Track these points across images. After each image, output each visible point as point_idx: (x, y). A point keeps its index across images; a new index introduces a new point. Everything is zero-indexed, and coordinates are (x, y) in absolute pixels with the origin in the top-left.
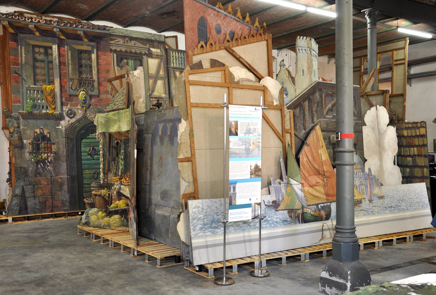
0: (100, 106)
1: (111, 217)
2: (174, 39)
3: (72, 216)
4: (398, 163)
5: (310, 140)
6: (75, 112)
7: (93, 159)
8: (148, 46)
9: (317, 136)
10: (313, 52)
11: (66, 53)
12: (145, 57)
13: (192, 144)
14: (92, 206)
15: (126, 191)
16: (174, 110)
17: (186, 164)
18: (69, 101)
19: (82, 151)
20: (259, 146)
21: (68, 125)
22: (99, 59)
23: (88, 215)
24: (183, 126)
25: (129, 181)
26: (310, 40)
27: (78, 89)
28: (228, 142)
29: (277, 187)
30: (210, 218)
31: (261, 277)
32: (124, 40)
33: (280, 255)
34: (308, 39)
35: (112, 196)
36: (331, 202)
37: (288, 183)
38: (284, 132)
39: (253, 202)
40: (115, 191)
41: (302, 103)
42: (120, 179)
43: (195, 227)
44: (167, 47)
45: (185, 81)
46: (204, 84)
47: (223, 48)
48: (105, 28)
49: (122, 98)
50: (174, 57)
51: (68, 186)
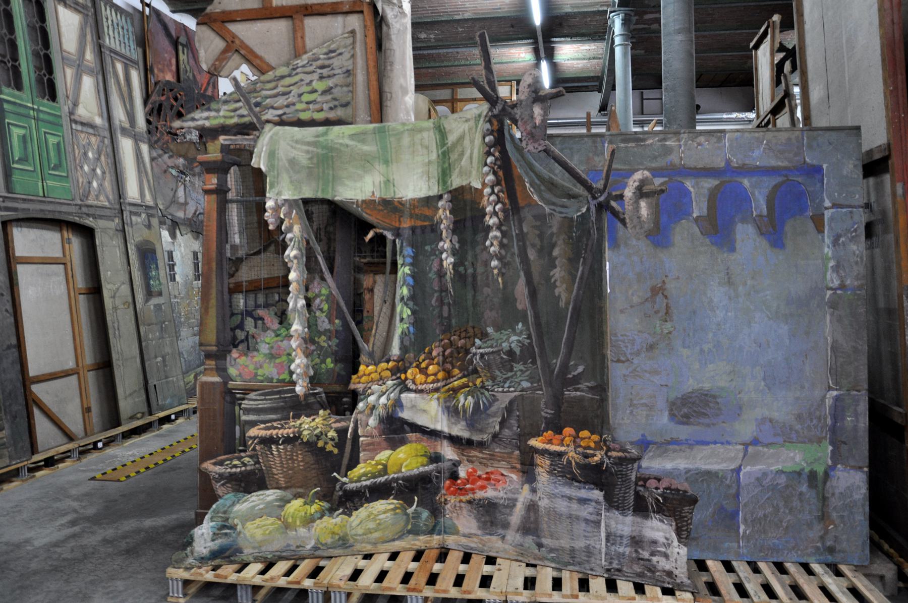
1: (355, 513)
35: (356, 436)
42: (399, 370)
49: (320, 86)
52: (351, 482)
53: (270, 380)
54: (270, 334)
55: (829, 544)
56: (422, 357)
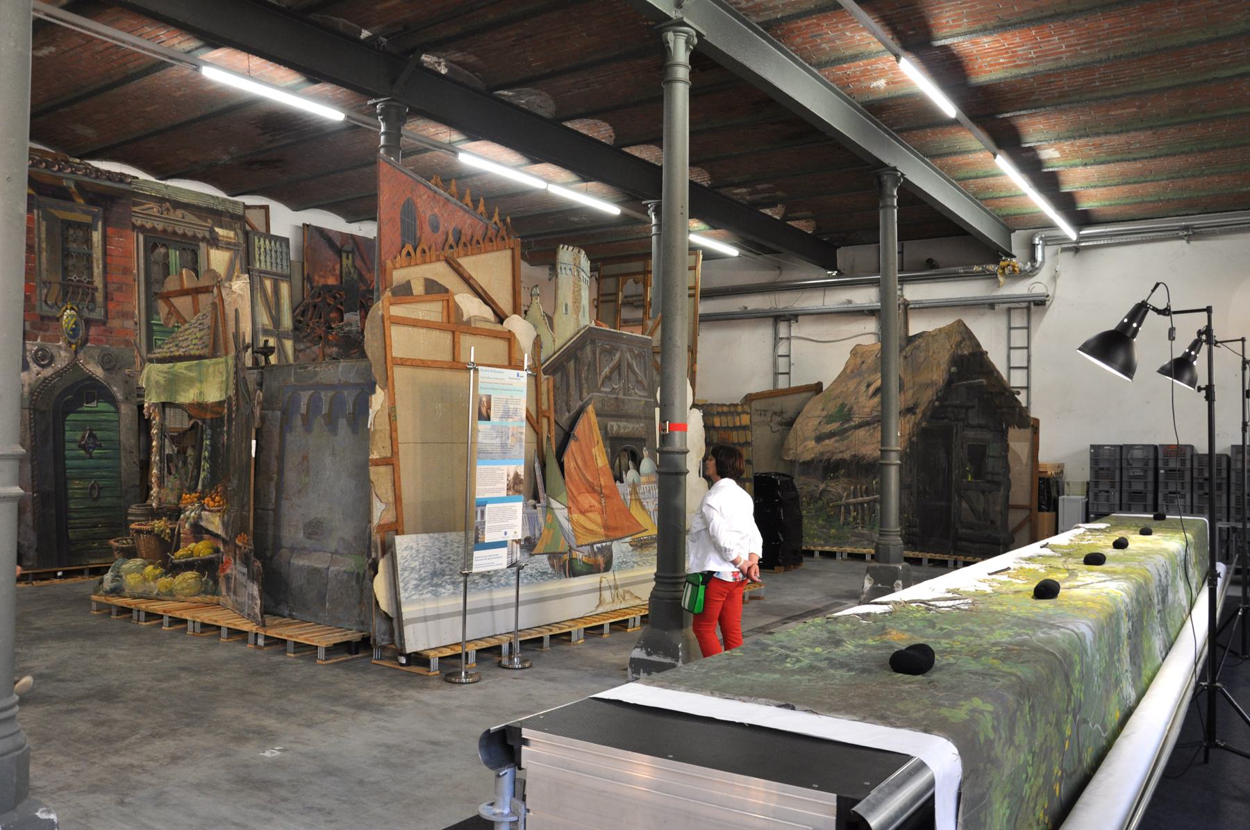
0: (107, 343)
1: (177, 577)
2: (263, 211)
3: (42, 580)
4: (703, 472)
5: (580, 429)
6: (52, 355)
7: (91, 458)
8: (210, 223)
9: (589, 423)
10: (582, 273)
11: (36, 226)
12: (203, 245)
13: (393, 433)
14: (130, 553)
15: (214, 523)
16: (338, 366)
17: (382, 469)
18: (40, 329)
19: (66, 438)
20: (521, 440)
21: (36, 381)
22: (108, 243)
23: (118, 572)
24: (378, 400)
25: (221, 503)
26: (579, 252)
27: (60, 304)
28: (475, 430)
29: (532, 514)
30: (430, 568)
31: (518, 669)
32: (161, 207)
33: (540, 633)
34: (576, 250)
35: (179, 533)
36: (612, 541)
37: (548, 507)
38: (540, 415)
39: (510, 538)
40: (186, 522)
41: (565, 363)
42: (200, 498)
43: (406, 585)
44: (248, 228)
45: (383, 316)
46: (415, 323)
47: (443, 258)
48: (122, 177)
49: (199, 335)
50: (262, 250)
51: (34, 514)
52: (176, 559)
53: (170, 503)
54: (172, 477)
55: (362, 619)
56: (213, 491)
